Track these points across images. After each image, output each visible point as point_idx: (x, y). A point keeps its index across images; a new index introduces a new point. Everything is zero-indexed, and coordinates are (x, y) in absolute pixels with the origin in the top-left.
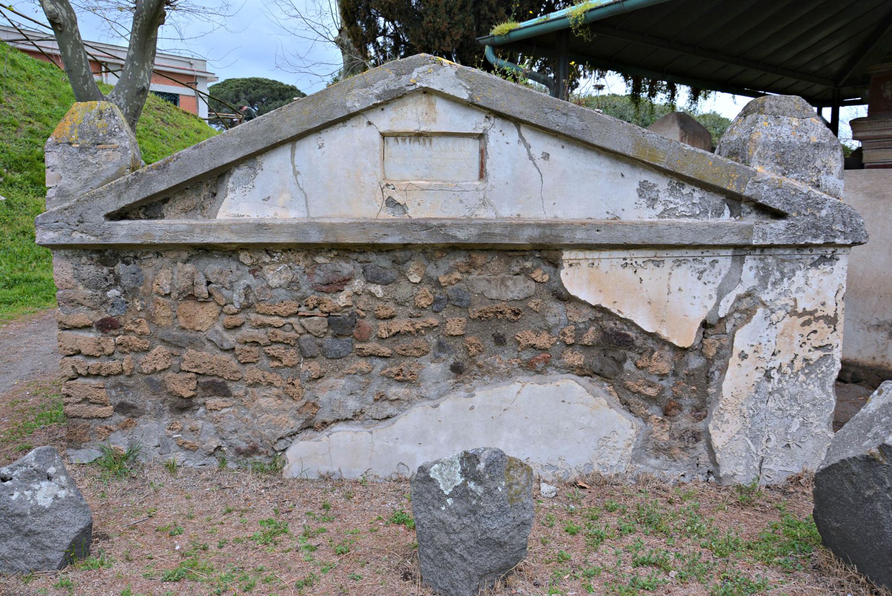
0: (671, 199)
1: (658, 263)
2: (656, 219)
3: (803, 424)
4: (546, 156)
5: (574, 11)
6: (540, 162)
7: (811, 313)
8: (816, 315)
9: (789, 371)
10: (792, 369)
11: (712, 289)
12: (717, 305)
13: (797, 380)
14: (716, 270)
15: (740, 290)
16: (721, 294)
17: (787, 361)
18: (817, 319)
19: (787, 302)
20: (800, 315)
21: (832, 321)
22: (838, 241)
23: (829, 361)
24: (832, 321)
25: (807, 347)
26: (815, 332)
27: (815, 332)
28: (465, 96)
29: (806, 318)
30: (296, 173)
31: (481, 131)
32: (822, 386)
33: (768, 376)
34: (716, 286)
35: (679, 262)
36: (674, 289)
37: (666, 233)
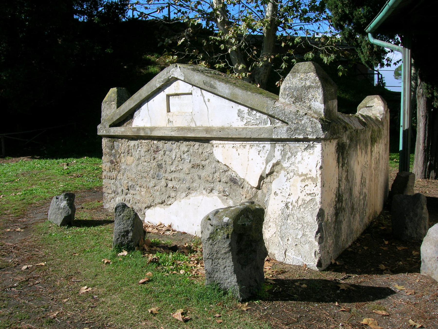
0: (249, 117)
1: (244, 147)
2: (244, 126)
3: (303, 235)
4: (209, 100)
5: (390, 3)
6: (207, 103)
7: (306, 175)
8: (308, 176)
9: (296, 204)
10: (298, 204)
11: (263, 160)
12: (266, 168)
13: (300, 210)
14: (265, 151)
15: (274, 161)
16: (267, 162)
17: (294, 200)
18: (308, 179)
19: (294, 168)
20: (300, 176)
21: (313, 180)
22: (310, 137)
23: (315, 202)
24: (313, 180)
25: (304, 193)
26: (307, 185)
27: (307, 185)
28: (183, 79)
29: (303, 177)
30: (148, 110)
31: (190, 92)
32: (312, 215)
33: (287, 206)
34: (265, 158)
35: (251, 146)
36: (250, 159)
37: (242, 132)
